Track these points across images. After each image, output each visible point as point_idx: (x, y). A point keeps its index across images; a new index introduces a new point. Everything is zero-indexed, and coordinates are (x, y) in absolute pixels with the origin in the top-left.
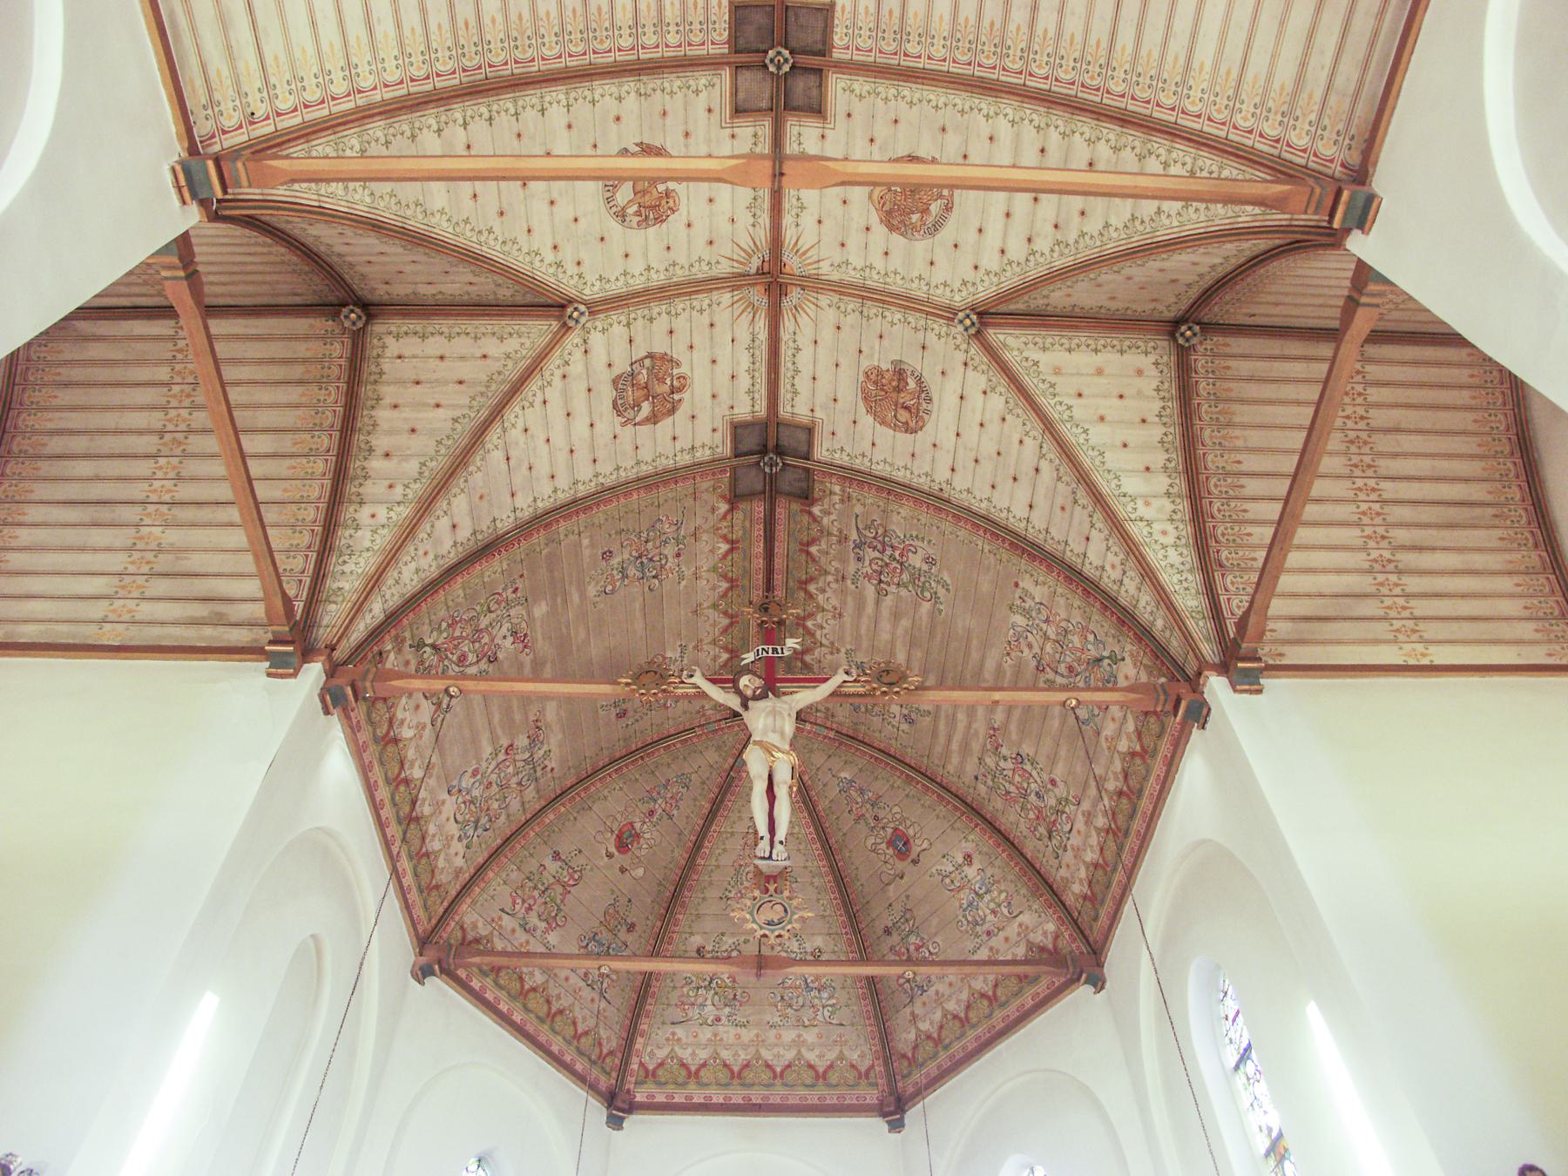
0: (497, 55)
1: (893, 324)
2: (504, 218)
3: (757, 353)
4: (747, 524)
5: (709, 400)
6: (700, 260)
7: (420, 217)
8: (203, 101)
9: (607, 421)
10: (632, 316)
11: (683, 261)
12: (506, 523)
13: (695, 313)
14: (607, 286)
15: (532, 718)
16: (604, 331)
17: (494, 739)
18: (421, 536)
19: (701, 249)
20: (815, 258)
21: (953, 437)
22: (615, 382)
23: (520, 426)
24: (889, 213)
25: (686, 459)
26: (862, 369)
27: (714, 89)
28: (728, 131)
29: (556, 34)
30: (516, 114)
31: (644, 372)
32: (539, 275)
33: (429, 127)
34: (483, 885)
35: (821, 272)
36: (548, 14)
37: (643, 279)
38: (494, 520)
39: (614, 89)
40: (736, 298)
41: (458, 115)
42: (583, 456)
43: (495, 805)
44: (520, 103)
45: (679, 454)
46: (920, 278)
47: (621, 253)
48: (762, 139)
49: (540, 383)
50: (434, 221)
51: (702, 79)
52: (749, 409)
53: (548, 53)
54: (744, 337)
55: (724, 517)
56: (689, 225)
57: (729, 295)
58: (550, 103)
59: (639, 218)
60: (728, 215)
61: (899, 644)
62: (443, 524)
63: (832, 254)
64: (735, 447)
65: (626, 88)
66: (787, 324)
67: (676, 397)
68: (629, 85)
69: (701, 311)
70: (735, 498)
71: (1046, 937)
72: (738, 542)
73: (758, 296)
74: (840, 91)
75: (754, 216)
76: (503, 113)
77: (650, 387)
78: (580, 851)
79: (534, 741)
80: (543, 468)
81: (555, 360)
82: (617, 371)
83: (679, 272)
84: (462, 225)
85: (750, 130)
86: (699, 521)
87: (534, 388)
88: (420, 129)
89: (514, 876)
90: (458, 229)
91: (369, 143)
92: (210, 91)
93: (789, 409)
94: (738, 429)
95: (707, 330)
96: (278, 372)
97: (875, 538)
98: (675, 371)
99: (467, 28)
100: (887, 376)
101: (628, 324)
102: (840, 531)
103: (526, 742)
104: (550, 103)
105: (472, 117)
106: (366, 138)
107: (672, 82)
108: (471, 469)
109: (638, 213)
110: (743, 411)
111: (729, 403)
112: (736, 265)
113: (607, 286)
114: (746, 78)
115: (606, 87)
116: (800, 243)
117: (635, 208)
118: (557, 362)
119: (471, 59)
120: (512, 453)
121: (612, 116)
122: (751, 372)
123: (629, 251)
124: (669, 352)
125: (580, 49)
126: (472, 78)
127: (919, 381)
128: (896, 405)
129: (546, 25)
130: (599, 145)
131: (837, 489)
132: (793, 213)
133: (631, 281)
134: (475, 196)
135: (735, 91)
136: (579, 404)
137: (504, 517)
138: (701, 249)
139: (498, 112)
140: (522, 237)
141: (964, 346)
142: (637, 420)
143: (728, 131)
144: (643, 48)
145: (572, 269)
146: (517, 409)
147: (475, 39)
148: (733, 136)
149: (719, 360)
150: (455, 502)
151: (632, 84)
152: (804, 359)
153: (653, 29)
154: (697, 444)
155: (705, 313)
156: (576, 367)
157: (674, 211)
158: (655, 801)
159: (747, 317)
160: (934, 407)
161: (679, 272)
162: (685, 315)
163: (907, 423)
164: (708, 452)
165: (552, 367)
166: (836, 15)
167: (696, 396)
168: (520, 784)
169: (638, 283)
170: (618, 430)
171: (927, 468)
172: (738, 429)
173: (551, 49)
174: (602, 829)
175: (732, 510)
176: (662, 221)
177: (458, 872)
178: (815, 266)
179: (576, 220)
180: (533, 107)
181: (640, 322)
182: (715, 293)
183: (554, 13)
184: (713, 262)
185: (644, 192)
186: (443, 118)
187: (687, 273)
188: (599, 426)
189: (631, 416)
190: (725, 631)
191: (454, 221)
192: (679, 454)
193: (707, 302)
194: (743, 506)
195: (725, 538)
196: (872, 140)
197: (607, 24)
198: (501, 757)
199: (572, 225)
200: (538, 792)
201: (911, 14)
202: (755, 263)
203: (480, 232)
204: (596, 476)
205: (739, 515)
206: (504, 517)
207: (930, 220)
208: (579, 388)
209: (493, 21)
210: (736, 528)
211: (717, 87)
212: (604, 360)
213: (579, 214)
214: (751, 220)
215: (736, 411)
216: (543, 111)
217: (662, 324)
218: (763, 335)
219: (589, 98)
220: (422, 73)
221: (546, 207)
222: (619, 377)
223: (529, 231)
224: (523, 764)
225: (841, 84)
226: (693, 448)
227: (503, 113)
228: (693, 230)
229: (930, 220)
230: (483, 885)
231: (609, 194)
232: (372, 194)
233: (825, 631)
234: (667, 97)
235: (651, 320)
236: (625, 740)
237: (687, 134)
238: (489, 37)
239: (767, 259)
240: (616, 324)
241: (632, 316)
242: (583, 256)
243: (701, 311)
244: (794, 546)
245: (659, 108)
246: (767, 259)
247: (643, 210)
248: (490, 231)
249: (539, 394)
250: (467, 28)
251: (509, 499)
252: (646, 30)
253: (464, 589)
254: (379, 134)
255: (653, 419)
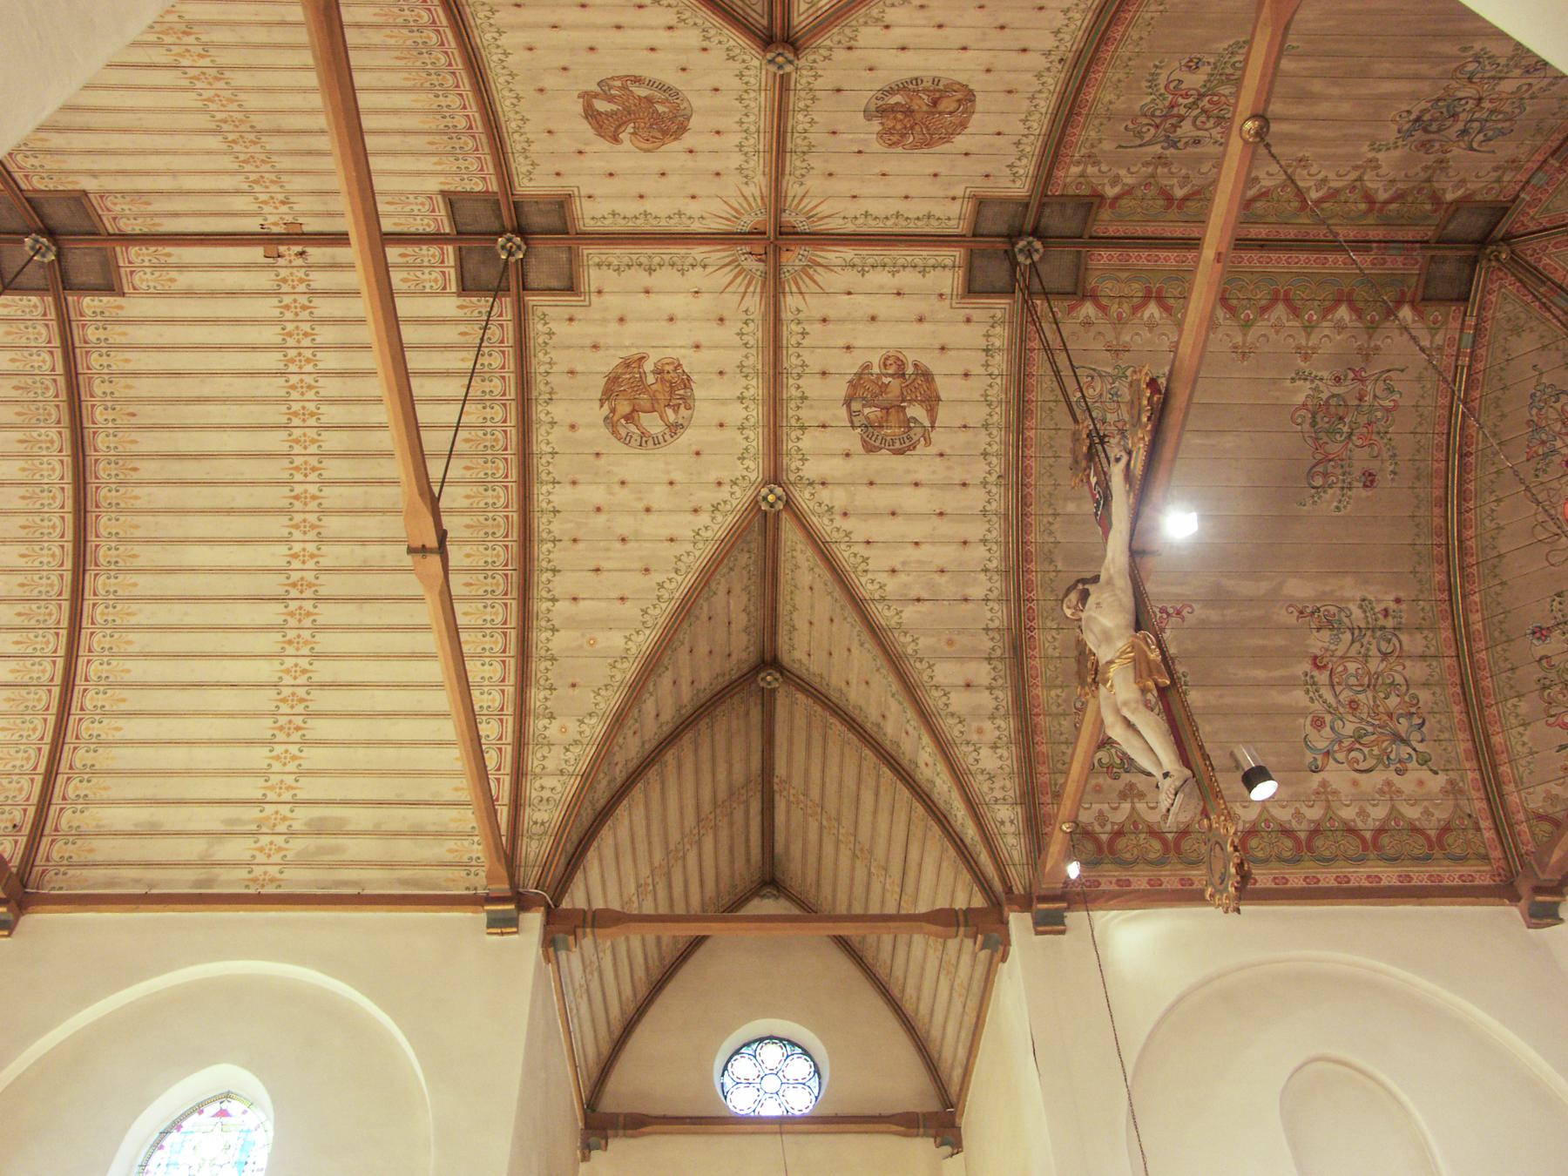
0: (498, 555)
1: (812, 122)
2: (652, 568)
3: (871, 261)
4: (1124, 275)
5: (927, 327)
6: (741, 334)
7: (626, 665)
8: (464, 874)
9: (920, 465)
10: (793, 422)
11: (737, 356)
12: (997, 615)
13: (805, 342)
14: (752, 451)
15: (1292, 620)
16: (803, 460)
17: (1288, 684)
18: (956, 733)
19: (727, 334)
20: (741, 200)
21: (969, 54)
22: (870, 449)
23: (883, 578)
24: (665, 133)
25: (1000, 362)
26: (885, 150)
27: (549, 313)
28: (594, 298)
29: (486, 490)
30: (554, 541)
31: (867, 411)
32: (721, 534)
33: (548, 640)
34: (1504, 757)
35: (757, 194)
36: (468, 497)
37: (752, 406)
38: (987, 629)
39: (542, 430)
40: (794, 289)
41: (545, 605)
42: (952, 501)
43: (1393, 701)
44: (544, 535)
45: (990, 370)
46: (741, 99)
47: (717, 431)
48: (604, 257)
49: (843, 546)
50: (634, 651)
51: (537, 328)
52: (948, 274)
53: (502, 500)
54: (847, 278)
55: (1103, 309)
56: (697, 347)
57: (789, 298)
58: (549, 502)
59: (682, 407)
60: (690, 298)
61: (1364, 91)
62: (959, 701)
63: (731, 186)
64: (1000, 293)
65: (542, 416)
66: (834, 225)
67: (910, 370)
68: (539, 412)
69: (804, 334)
70: (1079, 292)
71: (1103, 825)
72: (1149, 290)
73: (793, 259)
74: (531, 184)
75: (693, 266)
76: (551, 556)
77: (886, 404)
78: (1559, 595)
79: (1330, 624)
80: (946, 555)
81: (822, 525)
82: (857, 446)
83: (752, 360)
84: (647, 617)
85: (594, 272)
86: (1099, 345)
87: (846, 555)
88: (548, 650)
89: (1524, 707)
90: (649, 624)
91: (546, 708)
92: (459, 864)
93: (953, 223)
94: (972, 289)
95: (831, 326)
96: (817, 750)
97: (1157, 127)
98: (876, 370)
99: (471, 584)
100: (890, 124)
101: (803, 428)
102: (1146, 164)
103: (1325, 635)
104: (549, 502)
105: (549, 591)
106: (541, 711)
107: (539, 363)
108: (910, 651)
109: (676, 409)
110: (950, 282)
111: (934, 300)
112: (751, 289)
113: (752, 451)
114: (534, 279)
115: (540, 438)
116: (724, 215)
117: (670, 412)
118: (826, 521)
119: (498, 585)
120: (913, 594)
121: (570, 434)
122: (895, 269)
123: (716, 422)
124: (849, 378)
125: (501, 464)
126: (515, 586)
127: (891, 91)
128: (933, 113)
129: (476, 500)
130: (597, 450)
131: (1075, 170)
132: (689, 222)
133: (752, 421)
134: (622, 599)
135: (550, 290)
136: (883, 498)
137: (989, 615)
138: (727, 334)
139: (549, 561)
140: (677, 549)
141: (824, 52)
142: (927, 424)
143: (594, 298)
144: (504, 394)
145: (723, 494)
146: (863, 580)
147: (481, 577)
148: (599, 292)
149: (871, 312)
150: (939, 678)
151: (540, 408)
152: (876, 208)
153: (487, 383)
154: (983, 343)
155: (808, 328)
156: (837, 497)
157: (680, 365)
158: (1554, 451)
159: (822, 276)
160: (927, 75)
161: (752, 360)
162: (807, 356)
163: (959, 101)
164: (998, 329)
165: (828, 529)
166: (452, 189)
167: (910, 341)
168: (1385, 656)
169: (756, 413)
170: (933, 450)
171: (1029, 76)
172: (972, 289)
173: (498, 497)
174: (1547, 548)
175: (1094, 298)
176: (689, 379)
177: (1453, 789)
178: (751, 200)
179: (671, 483)
180: (550, 522)
181: (803, 413)
182: (783, 316)
183: (467, 490)
184: (745, 317)
185: (654, 399)
186: (543, 623)
187: (754, 351)
188: (920, 476)
189: (919, 431)
190: (1295, 311)
191: (641, 627)
192: (990, 370)
193: (793, 327)
194: (1092, 281)
195: (1135, 309)
196: (580, 152)
197: (480, 433)
198: (1322, 677)
199: (676, 488)
200: (1419, 629)
201: (426, 126)
202: (752, 264)
203: (659, 598)
204: (985, 484)
205: (1107, 288)
206: (989, 615)
207: (658, 95)
208: (866, 498)
209: (468, 556)
210: (1126, 292)
211: (547, 310)
212: (838, 462)
213: (666, 479)
214: (699, 269)
215: (947, 291)
216: (556, 512)
217: (812, 386)
218: (848, 253)
219: (548, 457)
220: (500, 639)
221: (652, 517)
222: (865, 444)
223: (672, 540)
224: (1357, 646)
225: (525, 182)
226: (987, 350)
227: (551, 556)
228: (703, 343)
229: (658, 95)
230: (1504, 757)
231: (650, 442)
232: (590, 715)
233: (1332, 176)
234: (555, 369)
235: (804, 398)
236: (1418, 478)
237: (595, 347)
238: (481, 563)
239: (748, 249)
240: (799, 444)
241: (793, 422)
242: (713, 476)
243: (804, 334)
244: (1172, 214)
245: (566, 378)
246: (748, 249)
247: (673, 402)
248: (661, 586)
249: (855, 549)
250: (471, 584)
251: (970, 606)
252: (487, 390)
253: (1050, 688)
254: (542, 695)
255: (932, 402)
